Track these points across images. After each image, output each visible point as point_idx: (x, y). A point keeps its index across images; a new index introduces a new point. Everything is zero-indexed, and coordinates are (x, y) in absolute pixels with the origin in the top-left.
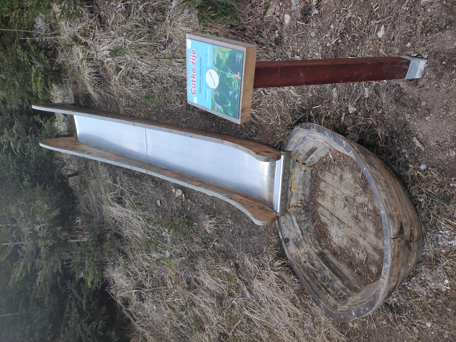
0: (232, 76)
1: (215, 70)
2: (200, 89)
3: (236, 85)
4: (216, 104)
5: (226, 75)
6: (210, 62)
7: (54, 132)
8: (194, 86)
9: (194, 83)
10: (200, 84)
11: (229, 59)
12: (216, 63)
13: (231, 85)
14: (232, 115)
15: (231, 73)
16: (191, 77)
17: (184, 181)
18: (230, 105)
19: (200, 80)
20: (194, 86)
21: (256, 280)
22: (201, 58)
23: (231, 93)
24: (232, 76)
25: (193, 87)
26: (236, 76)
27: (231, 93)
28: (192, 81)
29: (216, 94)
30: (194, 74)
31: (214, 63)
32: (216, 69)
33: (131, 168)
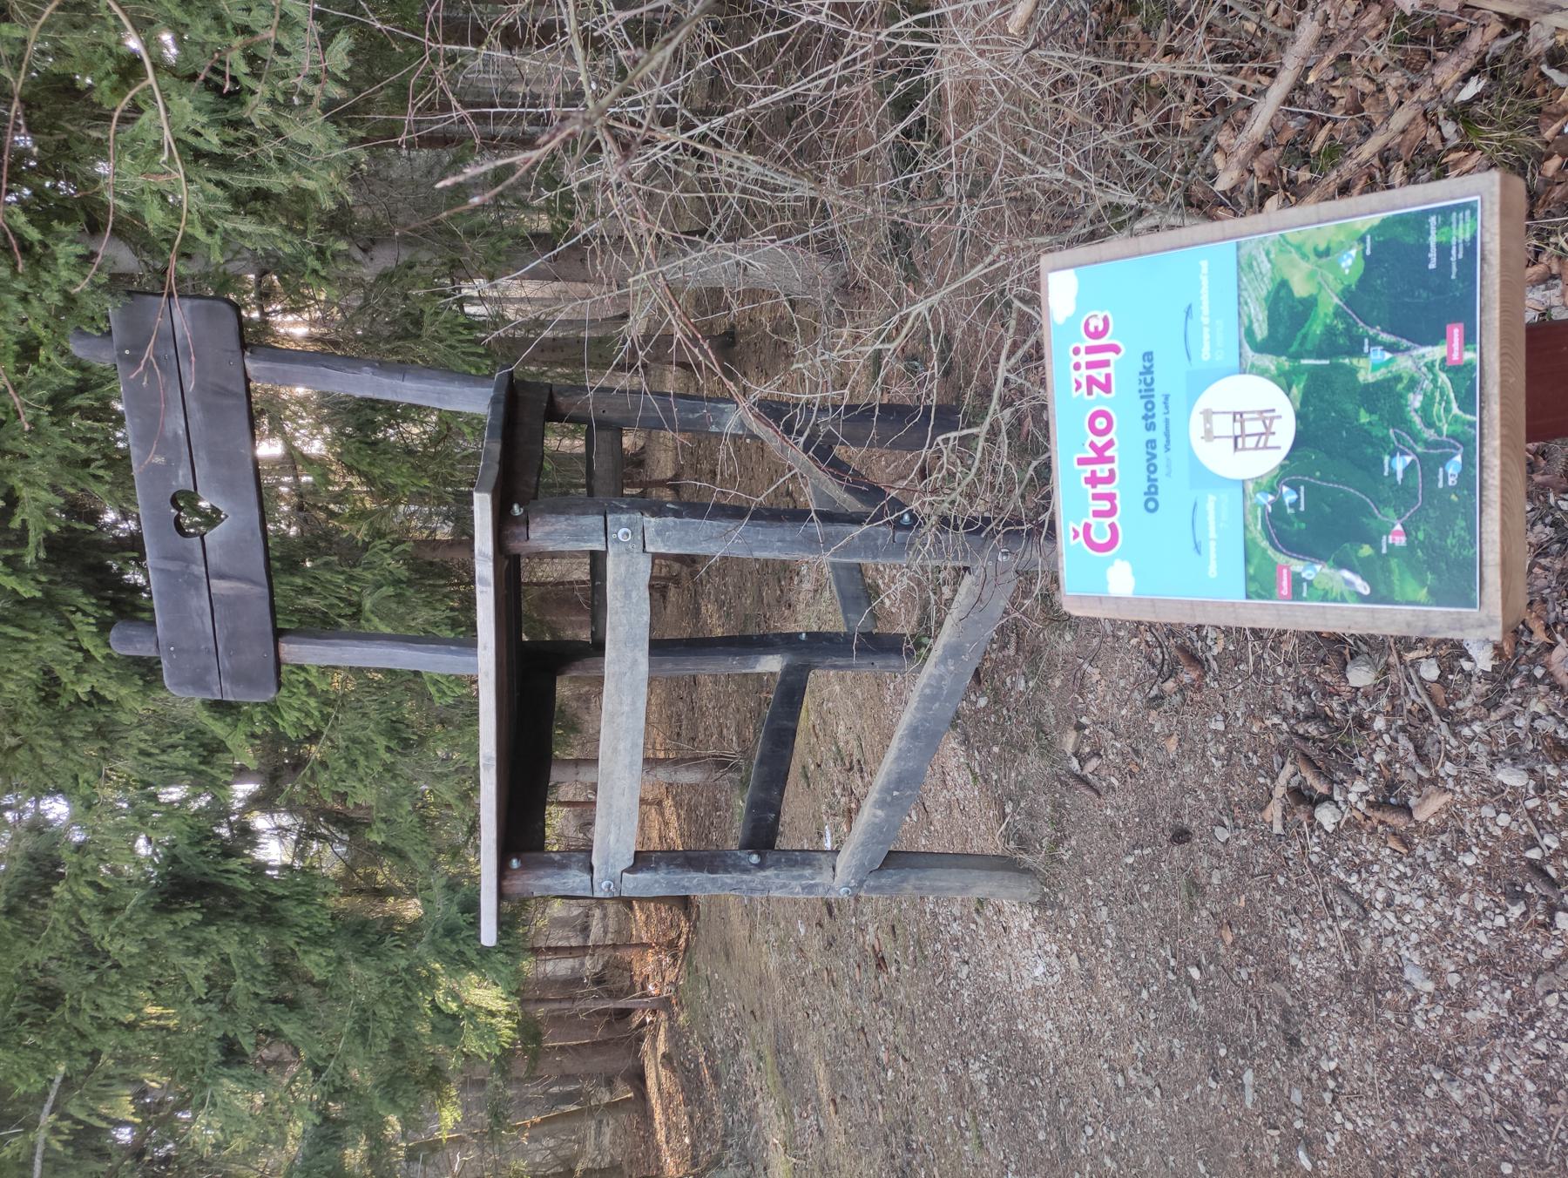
0: (1404, 364)
1: (1263, 373)
2: (1152, 492)
3: (1438, 409)
4: (1281, 559)
5: (1353, 372)
6: (1217, 335)
7: (323, 1137)
8: (1105, 505)
9: (1102, 489)
10: (1152, 468)
11: (1363, 281)
12: (1261, 331)
13: (1398, 418)
14: (1422, 594)
15: (1390, 348)
16: (1082, 461)
17: (855, 555)
18: (1401, 541)
19: (1151, 444)
20: (1105, 505)
21: (1524, 909)
22: (1148, 356)
23: (1400, 463)
24: (1404, 364)
25: (1097, 514)
26: (1436, 353)
27: (1400, 463)
28: (1093, 480)
29: (1278, 504)
30: (1100, 441)
31: (1250, 333)
32: (1268, 361)
33: (484, 582)
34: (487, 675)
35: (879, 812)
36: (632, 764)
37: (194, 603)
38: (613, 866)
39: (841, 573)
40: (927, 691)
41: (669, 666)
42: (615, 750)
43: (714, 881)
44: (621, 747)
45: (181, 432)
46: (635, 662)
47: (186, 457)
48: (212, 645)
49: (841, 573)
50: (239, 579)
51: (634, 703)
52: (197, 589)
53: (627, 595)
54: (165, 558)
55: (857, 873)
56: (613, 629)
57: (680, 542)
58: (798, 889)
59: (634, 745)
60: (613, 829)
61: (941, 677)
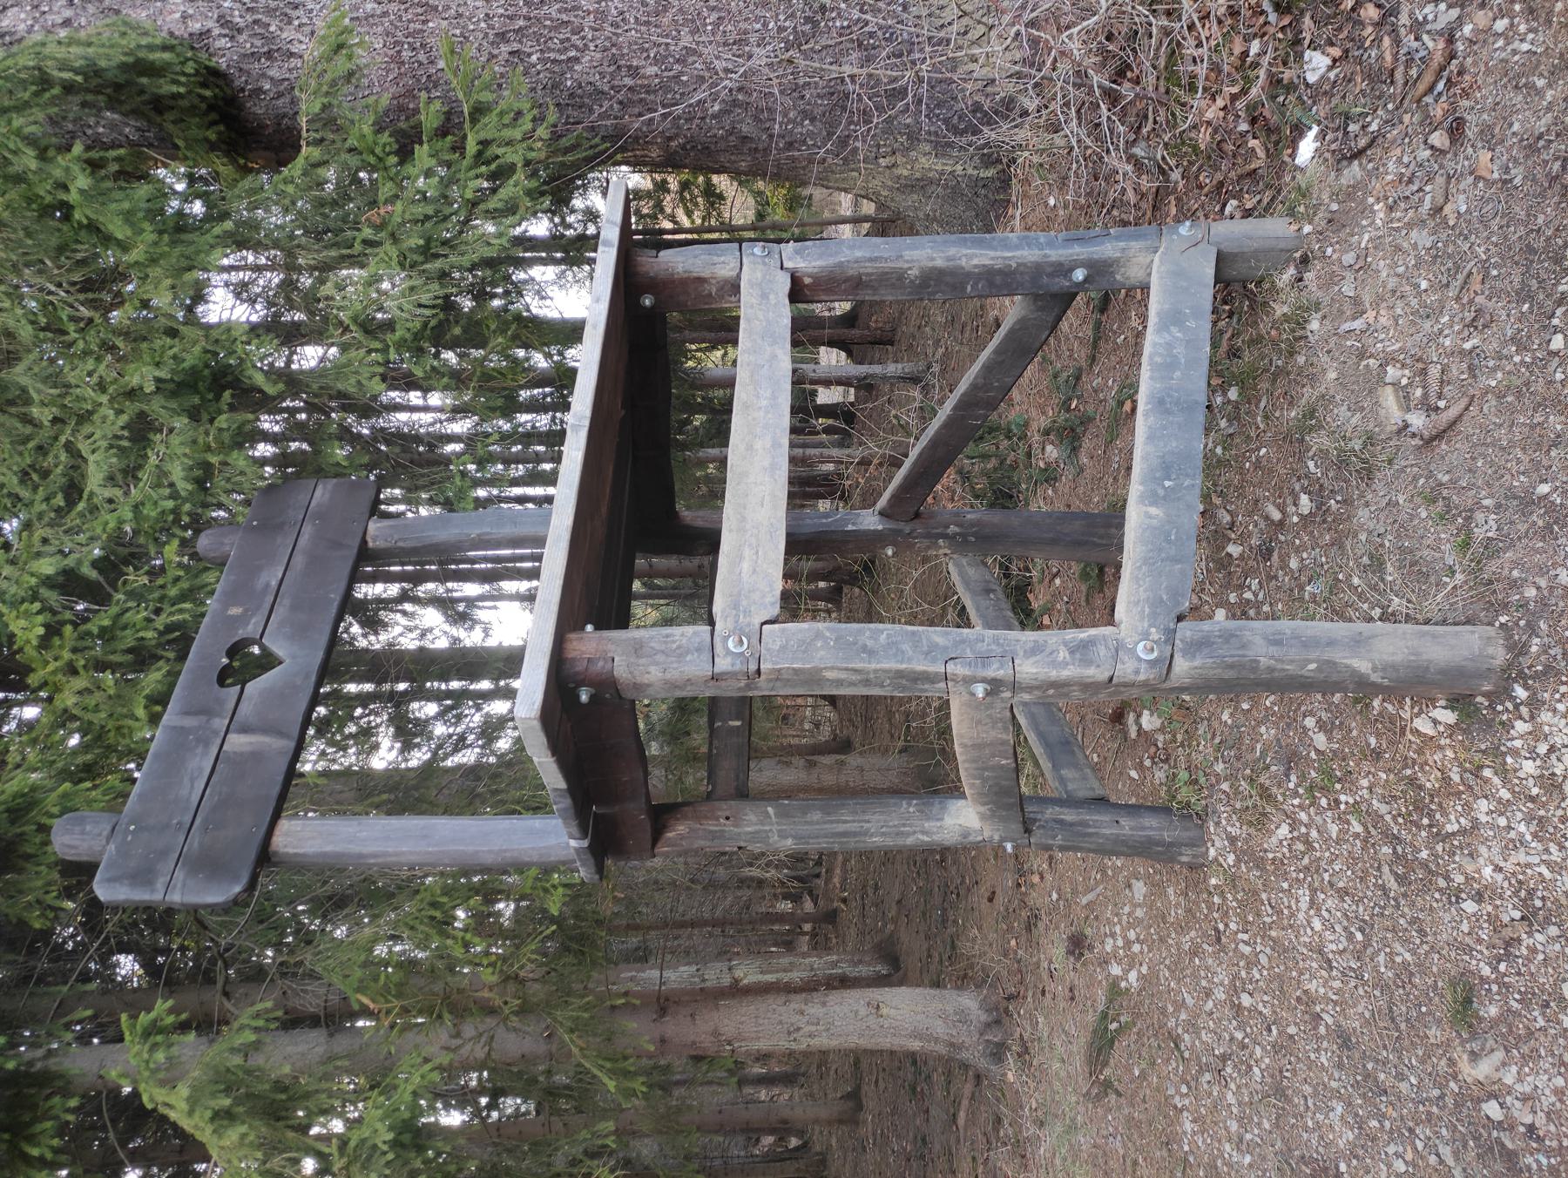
34: (595, 327)
35: (1153, 511)
36: (774, 467)
37: (192, 764)
38: (747, 613)
39: (1034, 709)
40: (1158, 359)
41: (816, 816)
42: (750, 447)
43: (915, 639)
44: (758, 445)
45: (274, 583)
46: (774, 357)
47: (267, 606)
48: (188, 819)
49: (1034, 709)
50: (264, 730)
51: (774, 397)
52: (207, 744)
53: (764, 296)
54: (187, 713)
55: (1154, 615)
56: (748, 320)
57: (820, 256)
58: (1063, 654)
59: (776, 445)
60: (747, 552)
61: (1169, 346)
